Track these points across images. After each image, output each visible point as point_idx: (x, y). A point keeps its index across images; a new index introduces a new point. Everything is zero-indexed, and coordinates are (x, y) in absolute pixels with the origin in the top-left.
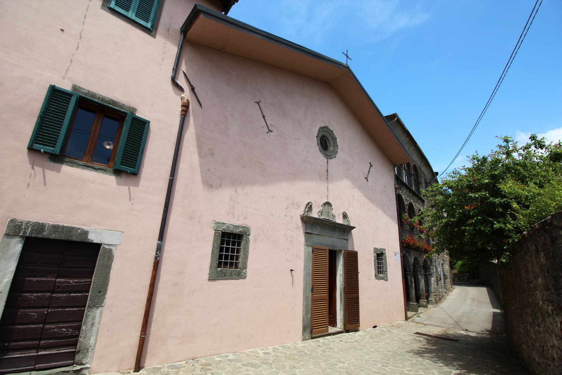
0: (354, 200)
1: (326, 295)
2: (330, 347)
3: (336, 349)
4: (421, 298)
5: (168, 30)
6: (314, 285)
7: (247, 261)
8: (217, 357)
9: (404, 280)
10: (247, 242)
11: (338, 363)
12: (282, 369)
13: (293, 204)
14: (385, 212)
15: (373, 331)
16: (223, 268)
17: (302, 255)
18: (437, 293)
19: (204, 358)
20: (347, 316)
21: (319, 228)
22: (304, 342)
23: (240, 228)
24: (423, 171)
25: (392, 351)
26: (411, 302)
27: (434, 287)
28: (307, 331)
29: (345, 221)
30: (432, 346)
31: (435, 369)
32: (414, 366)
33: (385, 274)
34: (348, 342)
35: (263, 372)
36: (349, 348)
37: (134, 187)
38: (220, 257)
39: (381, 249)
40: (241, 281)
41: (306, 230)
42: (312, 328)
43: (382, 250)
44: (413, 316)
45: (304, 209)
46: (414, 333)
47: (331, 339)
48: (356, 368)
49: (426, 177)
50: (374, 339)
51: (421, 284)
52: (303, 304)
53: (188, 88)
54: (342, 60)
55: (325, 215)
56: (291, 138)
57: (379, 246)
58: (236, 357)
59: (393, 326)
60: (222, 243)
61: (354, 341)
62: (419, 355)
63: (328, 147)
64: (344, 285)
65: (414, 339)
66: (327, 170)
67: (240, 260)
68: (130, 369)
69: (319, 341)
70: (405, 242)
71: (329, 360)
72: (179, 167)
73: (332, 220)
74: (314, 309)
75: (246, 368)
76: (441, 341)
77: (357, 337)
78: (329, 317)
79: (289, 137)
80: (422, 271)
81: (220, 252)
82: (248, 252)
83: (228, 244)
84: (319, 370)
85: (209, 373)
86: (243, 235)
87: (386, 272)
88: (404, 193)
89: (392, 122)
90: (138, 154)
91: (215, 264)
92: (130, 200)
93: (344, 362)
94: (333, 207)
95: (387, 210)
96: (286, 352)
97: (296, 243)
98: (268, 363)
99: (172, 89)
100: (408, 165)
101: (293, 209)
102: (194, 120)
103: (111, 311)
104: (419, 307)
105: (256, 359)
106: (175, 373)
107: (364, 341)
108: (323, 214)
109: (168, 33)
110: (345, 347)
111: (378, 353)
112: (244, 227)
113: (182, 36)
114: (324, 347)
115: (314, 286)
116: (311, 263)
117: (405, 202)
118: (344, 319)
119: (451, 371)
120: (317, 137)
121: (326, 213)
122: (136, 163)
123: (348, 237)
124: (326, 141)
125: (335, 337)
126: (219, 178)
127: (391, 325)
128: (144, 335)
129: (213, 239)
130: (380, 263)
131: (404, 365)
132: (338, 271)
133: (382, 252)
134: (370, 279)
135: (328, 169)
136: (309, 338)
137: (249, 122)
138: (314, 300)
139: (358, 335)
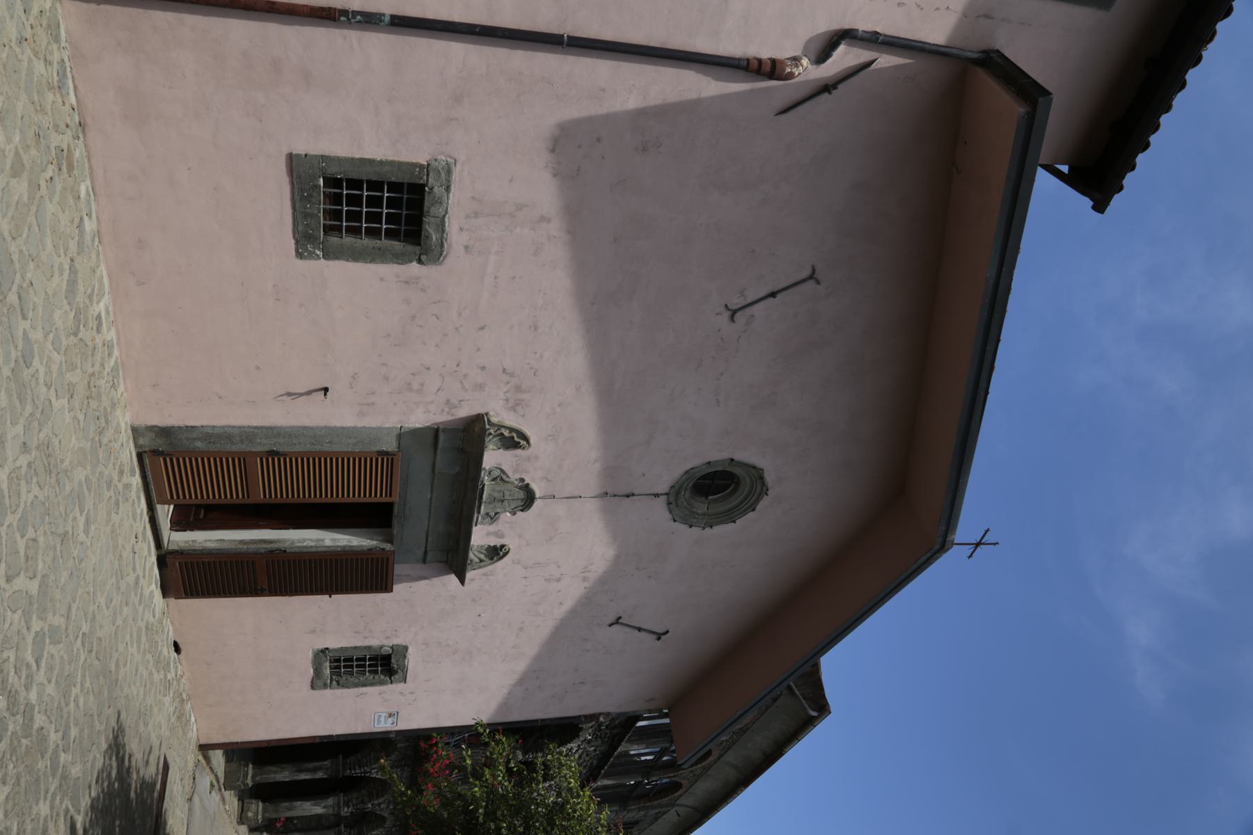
1: (260, 497)
3: (115, 518)
4: (267, 804)
5: (987, 16)
7: (347, 260)
8: (87, 188)
9: (318, 741)
10: (400, 258)
11: (84, 514)
13: (518, 389)
15: (165, 638)
16: (324, 192)
17: (371, 421)
19: (85, 154)
20: (204, 560)
22: (130, 431)
23: (438, 236)
24: (665, 816)
25: (118, 674)
26: (253, 768)
28: (159, 441)
29: (482, 553)
30: (136, 792)
33: (331, 683)
34: (134, 558)
35: (59, 311)
36: (121, 556)
38: (355, 184)
39: (404, 670)
40: (291, 243)
41: (444, 430)
43: (403, 671)
44: (211, 769)
45: (508, 423)
46: (167, 756)
48: (77, 562)
49: (646, 829)
50: (147, 635)
51: (309, 803)
52: (234, 427)
53: (830, 75)
54: (965, 530)
55: (494, 490)
56: (718, 379)
57: (413, 661)
58: (88, 238)
59: (182, 703)
60: (394, 187)
61: (138, 576)
63: (707, 499)
64: (293, 550)
65: (151, 748)
66: (633, 495)
67: (348, 240)
69: (133, 475)
70: (432, 746)
71: (90, 492)
72: (598, 57)
73: (479, 512)
74: (221, 459)
75: (67, 267)
77: (148, 588)
78: (199, 506)
79: (722, 374)
80: (348, 807)
82: (370, 262)
83: (392, 203)
85: (54, 170)
86: (420, 245)
87: (338, 684)
88: (585, 748)
89: (803, 701)
91: (334, 170)
94: (520, 514)
95: (527, 689)
96: (104, 379)
97: (404, 402)
98: (79, 327)
101: (505, 390)
102: (739, 95)
104: (241, 799)
105: (85, 292)
107: (140, 604)
108: (497, 483)
110: (123, 547)
112: (442, 245)
113: (976, 56)
114: (120, 486)
115: (285, 460)
116: (350, 450)
121: (499, 492)
126: (578, 170)
127: (184, 696)
129: (402, 160)
130: (364, 666)
133: (396, 672)
134: (313, 632)
136: (141, 446)
137: (753, 251)
138: (244, 459)
139: (152, 592)
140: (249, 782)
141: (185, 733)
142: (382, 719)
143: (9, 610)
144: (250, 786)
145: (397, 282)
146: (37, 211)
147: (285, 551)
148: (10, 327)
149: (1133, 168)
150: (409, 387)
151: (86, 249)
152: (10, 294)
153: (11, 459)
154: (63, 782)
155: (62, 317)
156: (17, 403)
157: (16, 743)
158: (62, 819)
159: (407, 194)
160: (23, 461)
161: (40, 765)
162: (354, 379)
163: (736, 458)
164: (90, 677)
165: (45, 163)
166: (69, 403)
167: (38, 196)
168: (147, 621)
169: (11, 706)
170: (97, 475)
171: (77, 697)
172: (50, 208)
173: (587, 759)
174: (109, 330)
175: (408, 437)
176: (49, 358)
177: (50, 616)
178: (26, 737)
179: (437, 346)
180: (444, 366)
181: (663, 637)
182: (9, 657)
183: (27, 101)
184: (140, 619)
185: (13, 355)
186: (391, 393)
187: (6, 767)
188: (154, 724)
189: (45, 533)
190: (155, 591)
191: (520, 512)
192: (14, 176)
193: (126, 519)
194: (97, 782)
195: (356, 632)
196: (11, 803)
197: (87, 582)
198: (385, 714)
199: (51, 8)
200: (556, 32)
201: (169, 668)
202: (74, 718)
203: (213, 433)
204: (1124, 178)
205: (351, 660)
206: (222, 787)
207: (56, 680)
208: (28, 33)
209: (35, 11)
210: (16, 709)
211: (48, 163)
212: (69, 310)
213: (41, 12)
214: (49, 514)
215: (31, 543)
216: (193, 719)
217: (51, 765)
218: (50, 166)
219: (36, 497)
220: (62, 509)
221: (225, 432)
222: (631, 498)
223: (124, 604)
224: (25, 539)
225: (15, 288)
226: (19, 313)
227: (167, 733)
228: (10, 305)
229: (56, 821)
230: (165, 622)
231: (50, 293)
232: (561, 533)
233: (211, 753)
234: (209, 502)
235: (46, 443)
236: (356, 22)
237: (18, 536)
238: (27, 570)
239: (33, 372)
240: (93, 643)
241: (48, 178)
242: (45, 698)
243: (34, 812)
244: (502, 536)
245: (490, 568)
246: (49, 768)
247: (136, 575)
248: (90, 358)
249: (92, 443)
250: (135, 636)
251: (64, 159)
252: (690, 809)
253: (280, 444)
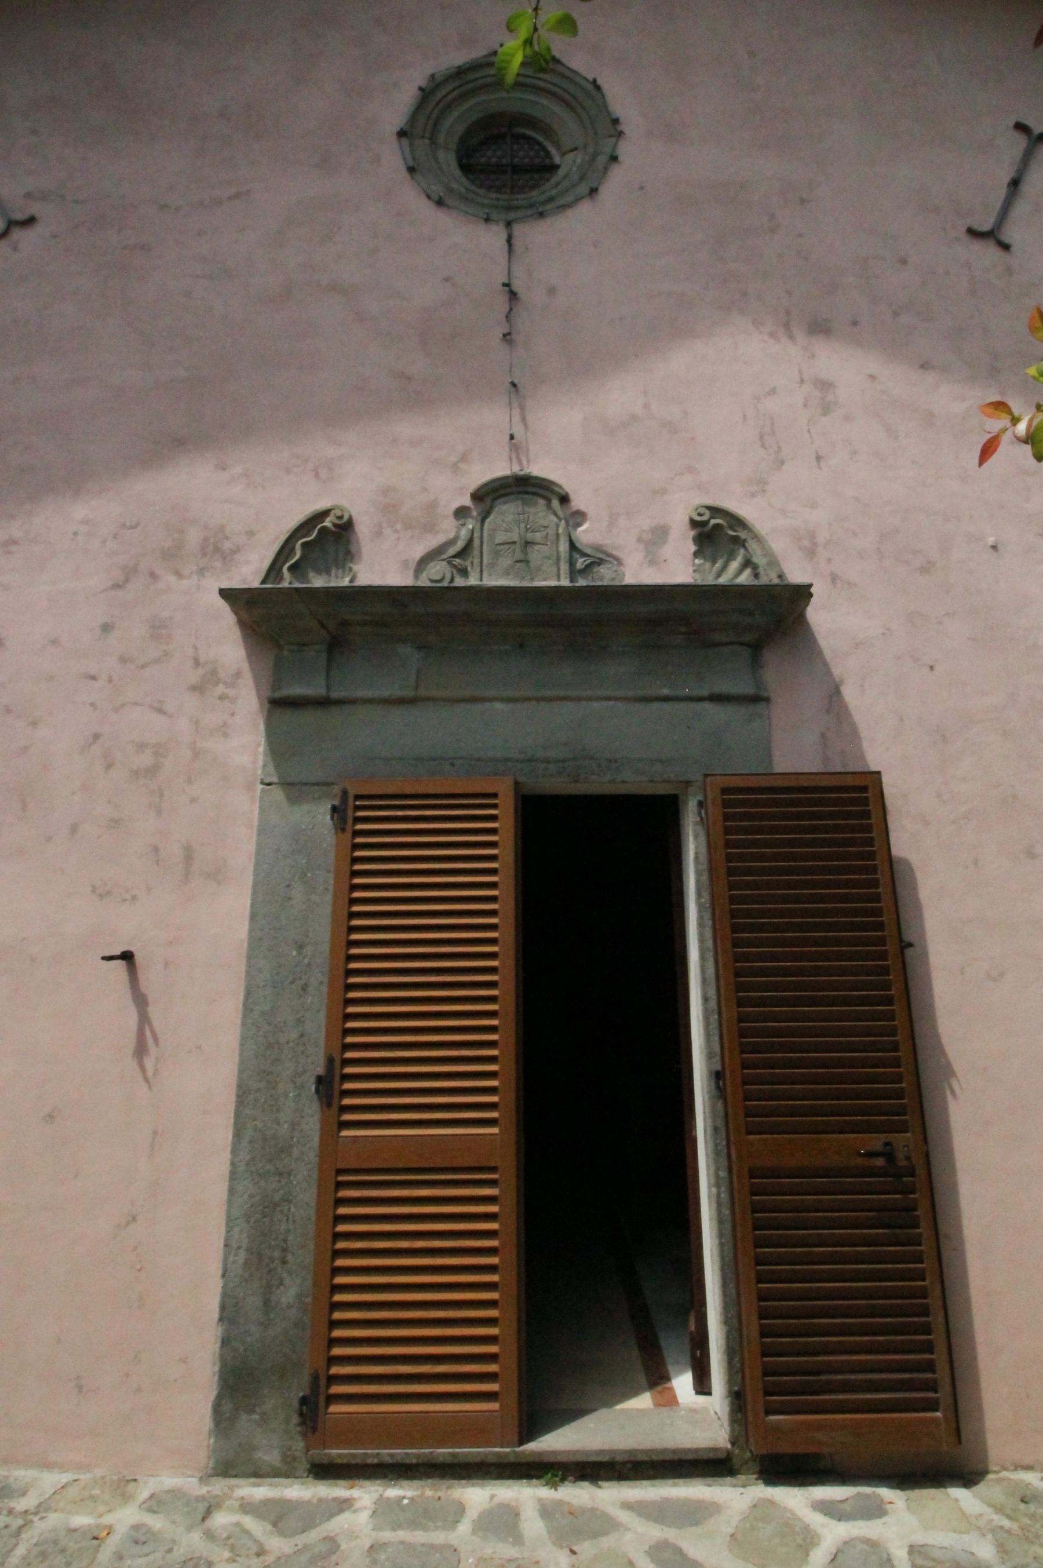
28: (268, 1406)
41: (277, 682)
52: (231, 1191)
162: (109, 893)
180: (92, 705)
203: (249, 1250)
221: (247, 1217)
232: (646, 406)
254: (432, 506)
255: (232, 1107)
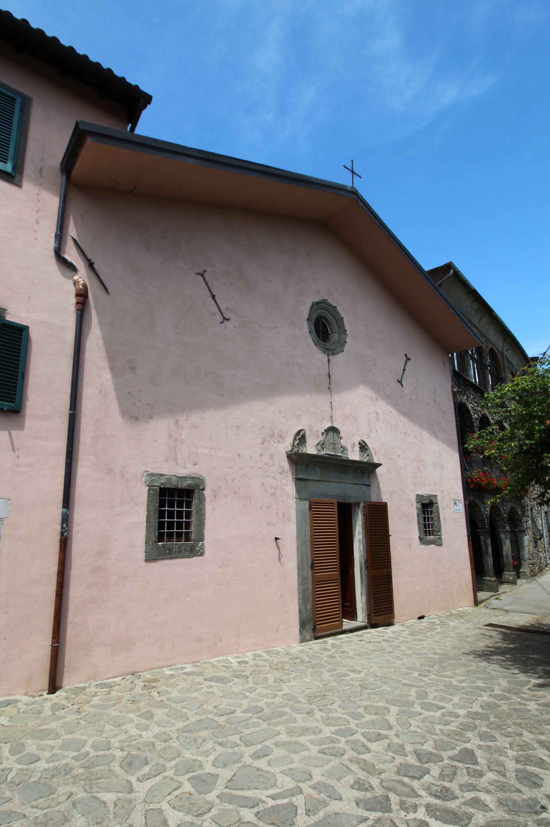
0: (378, 420)
1: (336, 573)
2: (343, 650)
3: (351, 653)
5: (41, 171)
6: (315, 559)
7: (204, 528)
8: (168, 670)
9: (471, 543)
10: (202, 500)
11: (349, 673)
12: (262, 684)
13: (272, 436)
14: (434, 434)
16: (167, 542)
17: (293, 514)
18: (535, 561)
19: (149, 672)
20: (372, 603)
21: (320, 470)
22: (303, 644)
23: (188, 480)
24: (509, 358)
25: (441, 653)
26: (486, 576)
27: (529, 551)
28: (308, 628)
30: (509, 644)
31: (504, 677)
32: (470, 675)
34: (373, 642)
36: (372, 650)
37: (17, 431)
38: (161, 525)
39: (429, 496)
41: (296, 475)
42: (315, 623)
43: (430, 497)
44: (488, 599)
45: (291, 441)
47: (347, 639)
48: (377, 679)
50: (416, 635)
52: (299, 588)
55: (329, 448)
56: (263, 327)
57: (425, 492)
58: (196, 669)
61: (383, 640)
62: (484, 658)
63: (330, 334)
64: (366, 556)
66: (329, 373)
67: (193, 528)
68: (43, 690)
69: (326, 642)
70: (472, 482)
72: (82, 394)
73: (341, 456)
74: (317, 594)
76: (526, 635)
78: (343, 606)
79: (260, 326)
80: (506, 526)
81: (159, 519)
82: (204, 516)
83: (171, 505)
84: (319, 684)
85: (154, 691)
86: (194, 490)
87: (439, 531)
90: (17, 380)
91: (154, 537)
92: (14, 450)
93: (360, 671)
94: (341, 435)
95: (439, 430)
96: (273, 660)
98: (243, 675)
99: (57, 269)
100: (479, 351)
101: (273, 443)
102: (99, 316)
103: (6, 612)
104: (502, 583)
106: (105, 693)
108: (325, 447)
109: (42, 177)
110: (367, 649)
111: (418, 657)
112: (194, 478)
113: (64, 177)
114: (333, 650)
117: (472, 414)
118: (367, 609)
119: (528, 681)
120: (308, 319)
121: (329, 446)
122: (15, 395)
123: (369, 481)
124: (326, 325)
125: (353, 636)
126: (148, 404)
127: (448, 614)
128: (56, 643)
129: (146, 500)
130: (428, 518)
131: (454, 673)
132: (356, 536)
134: (410, 545)
135: (330, 373)
136: (311, 638)
137: (189, 308)
138: (316, 582)
139: (391, 631)
140: (494, 579)
141: (469, 614)
142: (458, 508)
143: (410, 728)
144: (496, 578)
145: (215, 502)
146: (175, 702)
147: (366, 560)
148: (238, 722)
149: (124, 79)
150: (273, 494)
151: (201, 671)
152: (219, 722)
153: (317, 724)
154: (513, 692)
155: (236, 686)
156: (284, 718)
157: (494, 726)
158: (536, 693)
159: (166, 497)
160: (318, 715)
161: (505, 708)
163: (306, 316)
164: (445, 672)
165: (150, 697)
166: (286, 683)
167: (167, 702)
168: (408, 635)
169: (471, 729)
170: (327, 664)
171: (457, 681)
172: (175, 693)
173: (477, 399)
174: (247, 656)
175: (300, 495)
176: (259, 695)
177: (410, 698)
178: (489, 718)
179: (250, 479)
181: (408, 357)
182: (440, 729)
183: (113, 708)
184: (407, 639)
185: (255, 720)
186: (277, 504)
187: (511, 733)
188: (467, 632)
189: (361, 700)
190: (390, 630)
191: (341, 434)
192: (152, 717)
193: (351, 647)
194: (508, 669)
195: (410, 522)
196: (533, 730)
197: (388, 672)
198: (455, 506)
199: (66, 692)
200: (68, 418)
201: (433, 622)
202: (471, 683)
204: (130, 84)
205: (425, 525)
206: (497, 593)
207: (450, 695)
208: (76, 707)
209: (65, 702)
210: (472, 725)
211: (150, 695)
212: (233, 682)
213: (66, 698)
214: (350, 697)
215: (367, 711)
216: (460, 609)
217: (504, 700)
218: (151, 694)
219: (339, 706)
220: (347, 688)
221: (302, 592)
222: (331, 375)
223: (399, 648)
224: (365, 715)
225: (216, 718)
226: (231, 715)
227: (471, 624)
228: (226, 721)
229: (538, 697)
230: (408, 625)
231: (222, 694)
232: (351, 412)
233: (479, 599)
234: (340, 601)
235: (308, 698)
236: (67, 527)
237: (363, 720)
238: (384, 714)
239: (266, 706)
240: (424, 669)
241: (158, 695)
242: (462, 703)
243: (536, 713)
244: (354, 444)
245: (372, 450)
246: (505, 702)
247: (382, 641)
248: (261, 668)
249: (309, 667)
250: (417, 643)
251: (149, 685)
252: (505, 343)
253: (307, 563)
254: (318, 431)
255: (297, 571)
